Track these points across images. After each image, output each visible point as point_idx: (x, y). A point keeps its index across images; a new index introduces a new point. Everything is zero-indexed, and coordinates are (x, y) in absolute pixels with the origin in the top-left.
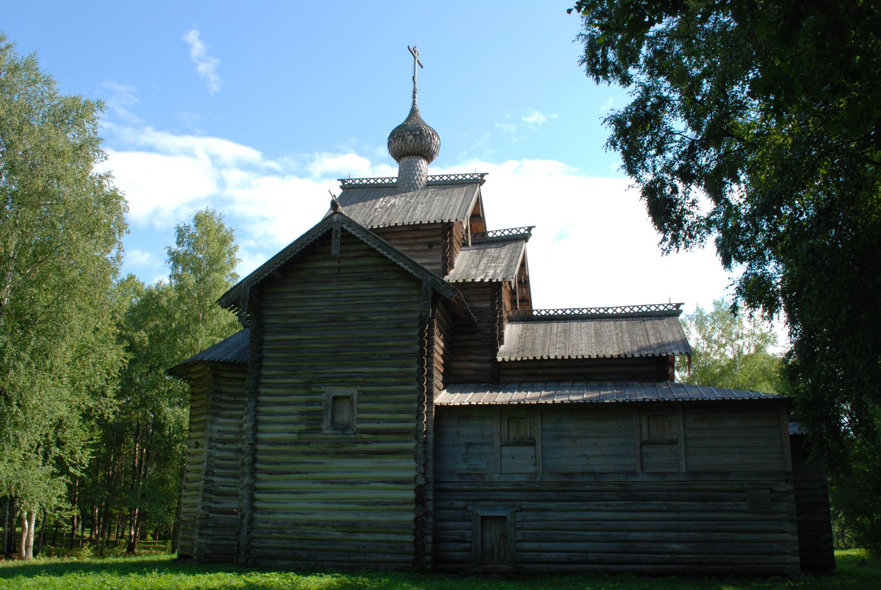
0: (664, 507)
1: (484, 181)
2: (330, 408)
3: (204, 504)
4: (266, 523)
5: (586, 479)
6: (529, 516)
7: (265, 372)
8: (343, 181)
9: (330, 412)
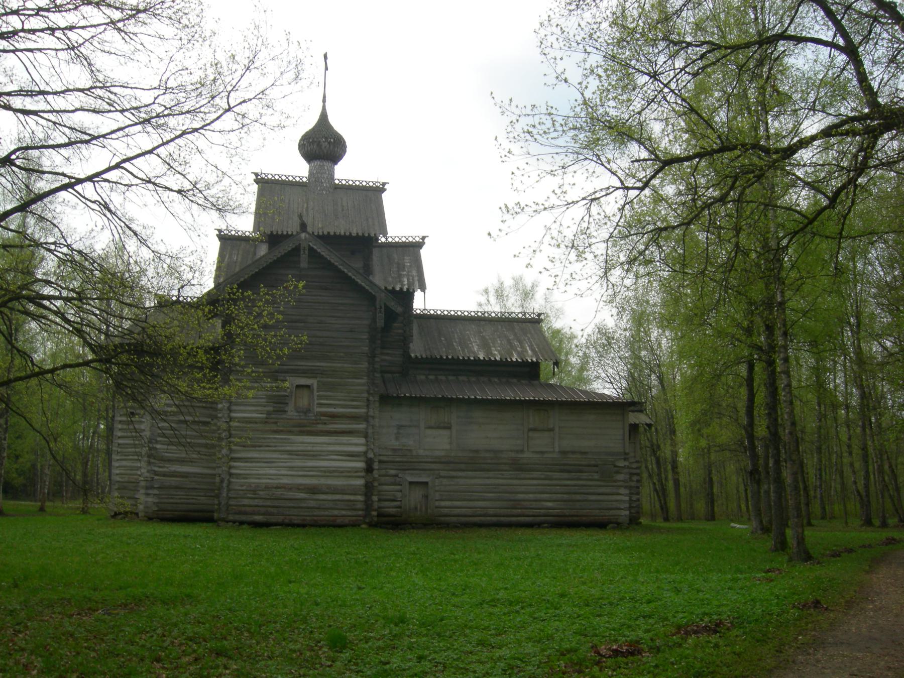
0: (543, 476)
1: (386, 190)
2: (294, 394)
3: (149, 468)
4: (242, 486)
5: (487, 455)
6: (445, 481)
7: (365, 388)
8: (256, 174)
9: (293, 397)
